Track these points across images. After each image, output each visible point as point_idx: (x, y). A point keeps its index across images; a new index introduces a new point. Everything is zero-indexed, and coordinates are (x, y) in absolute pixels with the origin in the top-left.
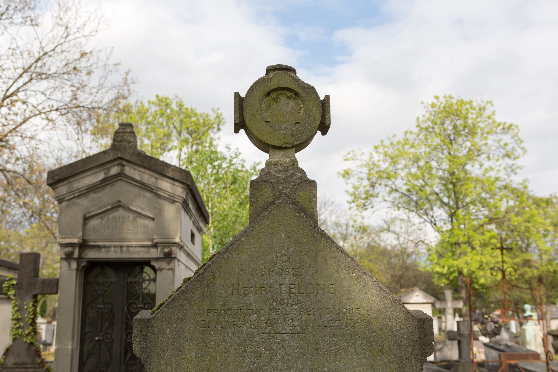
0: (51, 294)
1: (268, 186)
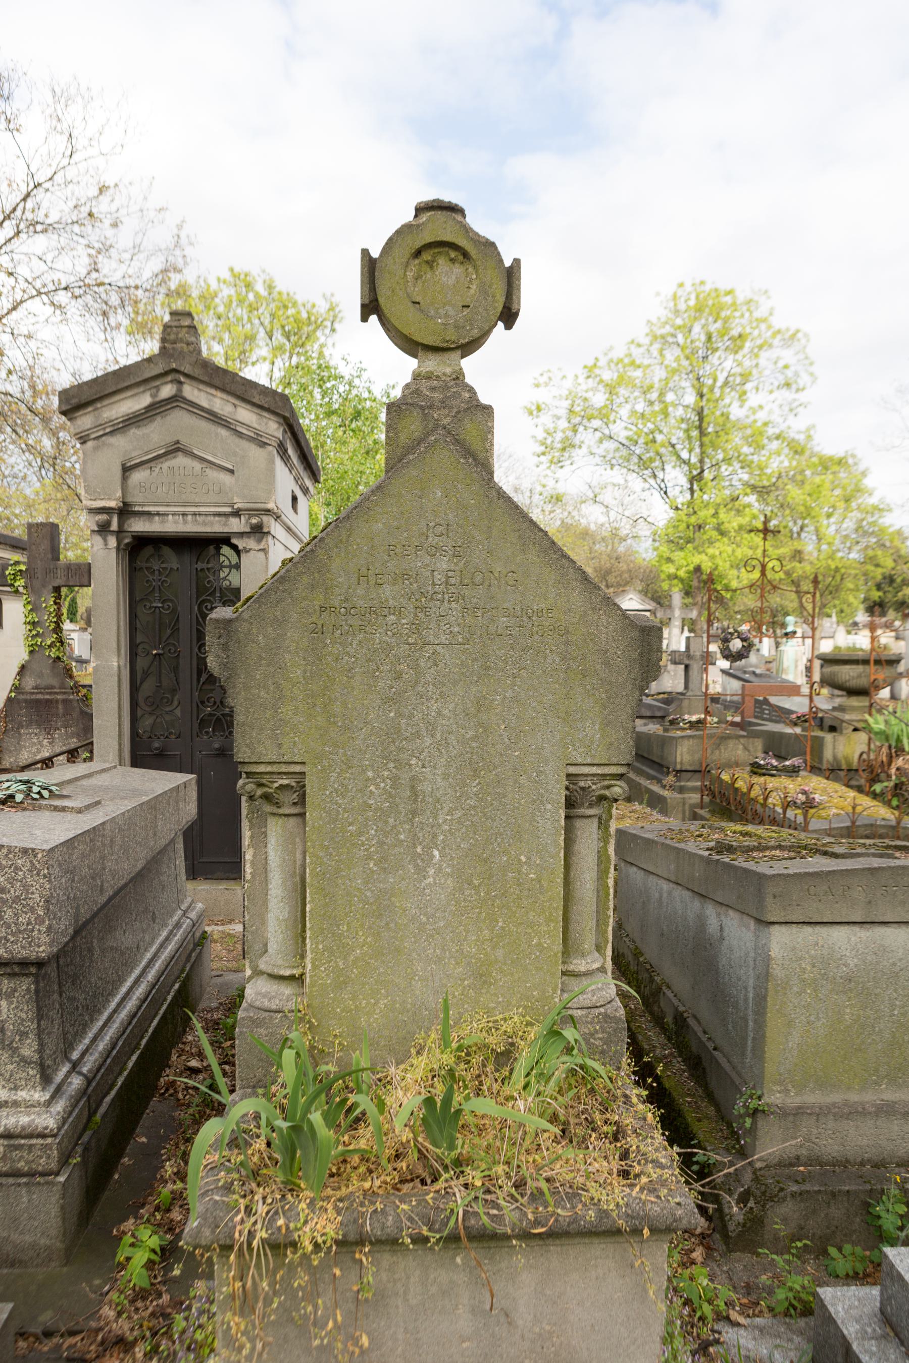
0: (81, 586)
1: (416, 412)
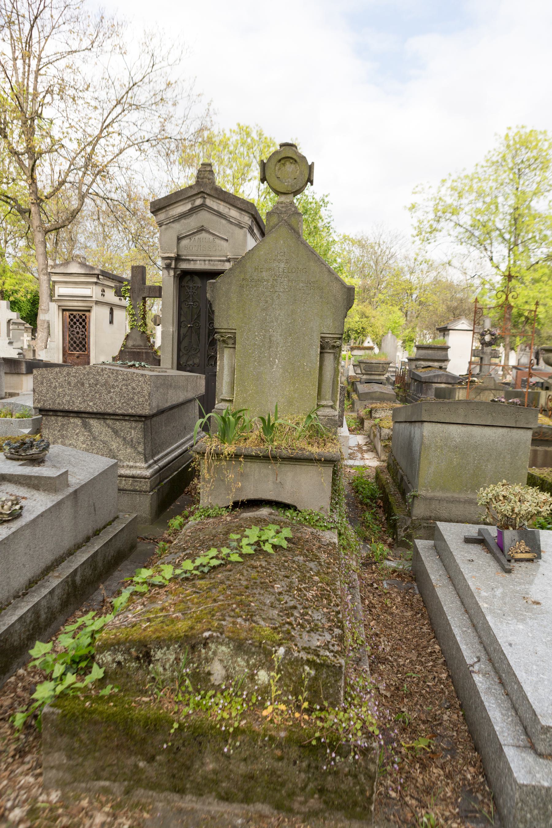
1: (276, 215)
